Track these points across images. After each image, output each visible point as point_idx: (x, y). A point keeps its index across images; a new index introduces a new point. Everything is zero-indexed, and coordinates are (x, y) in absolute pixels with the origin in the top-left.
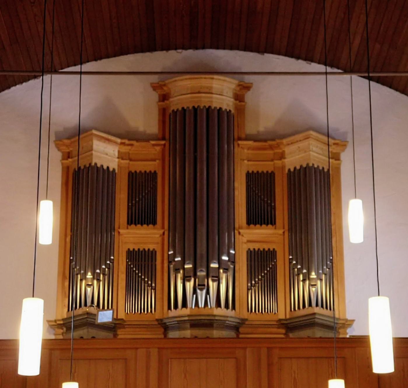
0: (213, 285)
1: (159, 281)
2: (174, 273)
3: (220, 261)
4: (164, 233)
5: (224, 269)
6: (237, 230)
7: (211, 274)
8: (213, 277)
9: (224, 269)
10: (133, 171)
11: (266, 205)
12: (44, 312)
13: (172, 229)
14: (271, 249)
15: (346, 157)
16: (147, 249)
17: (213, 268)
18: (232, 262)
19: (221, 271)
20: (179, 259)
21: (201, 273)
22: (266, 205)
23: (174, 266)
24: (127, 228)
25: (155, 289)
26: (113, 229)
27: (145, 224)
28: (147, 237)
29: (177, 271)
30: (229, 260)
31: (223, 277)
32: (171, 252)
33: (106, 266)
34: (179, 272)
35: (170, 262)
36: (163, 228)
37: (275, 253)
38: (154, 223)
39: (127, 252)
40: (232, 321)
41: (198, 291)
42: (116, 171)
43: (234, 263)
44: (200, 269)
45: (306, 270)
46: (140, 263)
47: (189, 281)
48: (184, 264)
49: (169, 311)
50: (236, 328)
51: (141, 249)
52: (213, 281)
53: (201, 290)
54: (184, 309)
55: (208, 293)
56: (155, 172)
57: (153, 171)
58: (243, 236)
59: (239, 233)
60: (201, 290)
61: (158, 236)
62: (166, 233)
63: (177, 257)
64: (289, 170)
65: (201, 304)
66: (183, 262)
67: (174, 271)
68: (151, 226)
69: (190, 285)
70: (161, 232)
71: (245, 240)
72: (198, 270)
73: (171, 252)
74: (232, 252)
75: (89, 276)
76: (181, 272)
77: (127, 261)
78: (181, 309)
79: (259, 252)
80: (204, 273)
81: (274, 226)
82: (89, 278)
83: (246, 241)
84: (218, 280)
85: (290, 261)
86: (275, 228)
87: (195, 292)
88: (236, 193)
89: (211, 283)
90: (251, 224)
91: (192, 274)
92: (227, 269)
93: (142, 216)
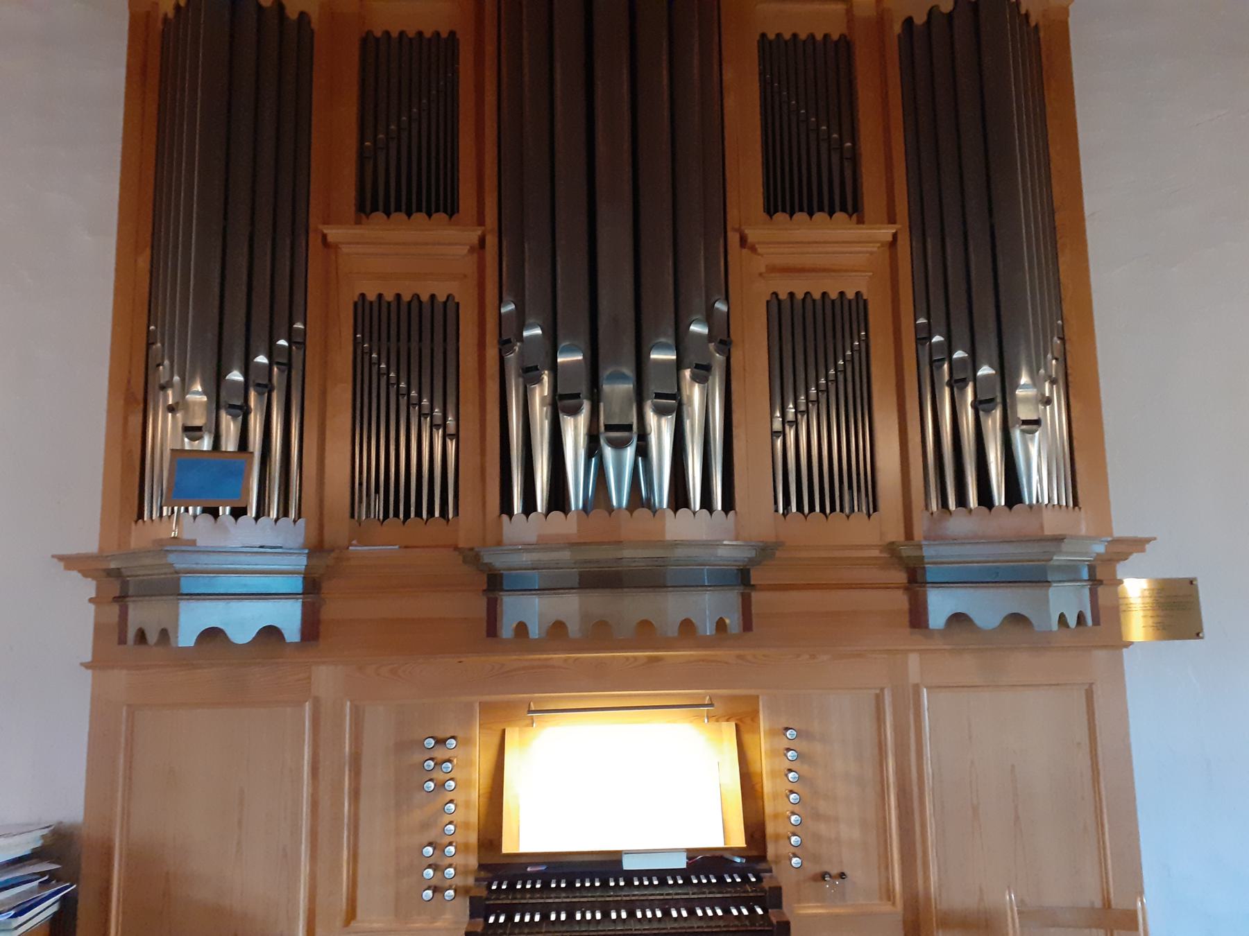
0: (661, 431)
1: (469, 409)
2: (521, 380)
3: (680, 342)
4: (482, 241)
5: (698, 366)
6: (735, 230)
7: (653, 387)
8: (658, 396)
9: (698, 366)
10: (378, 34)
11: (824, 146)
12: (102, 524)
13: (511, 228)
14: (850, 295)
15: (487, 559)
16: (425, 298)
17: (657, 362)
18: (722, 342)
19: (687, 373)
20: (512, 307)
21: (618, 390)
22: (824, 146)
23: (521, 355)
24: (358, 222)
25: (456, 436)
26: (298, 229)
27: (419, 210)
28: (425, 257)
29: (530, 375)
30: (710, 337)
31: (695, 394)
32: (509, 308)
33: (270, 357)
34: (539, 380)
35: (505, 345)
36: (481, 222)
37: (861, 307)
38: (451, 209)
39: (356, 304)
40: (730, 552)
41: (608, 452)
42: (315, 25)
43: (725, 345)
44: (608, 372)
45: (991, 366)
46: (414, 345)
47: (574, 412)
48: (522, 326)
49: (505, 517)
50: (742, 578)
51: (406, 297)
52: (661, 412)
53: (619, 445)
54: (557, 515)
55: (643, 451)
56: (452, 34)
57: (444, 35)
58: (753, 249)
59: (743, 241)
60: (619, 445)
61: (465, 250)
62: (491, 241)
63: (532, 326)
64: (909, 21)
65: (619, 495)
66: (552, 344)
67: (519, 376)
68: (441, 217)
69: (574, 431)
70: (473, 235)
71: (760, 264)
72: (605, 373)
73: (509, 308)
74: (721, 306)
75: (197, 395)
76: (546, 378)
77: (355, 338)
78: (546, 515)
79: (828, 304)
80: (628, 387)
81: (855, 216)
82: (195, 403)
83: (763, 269)
84: (675, 407)
85: (923, 338)
86: (860, 221)
87: (593, 448)
88: (730, 102)
89: (651, 418)
90: (776, 211)
91: (583, 388)
92: (707, 368)
93: (408, 183)
